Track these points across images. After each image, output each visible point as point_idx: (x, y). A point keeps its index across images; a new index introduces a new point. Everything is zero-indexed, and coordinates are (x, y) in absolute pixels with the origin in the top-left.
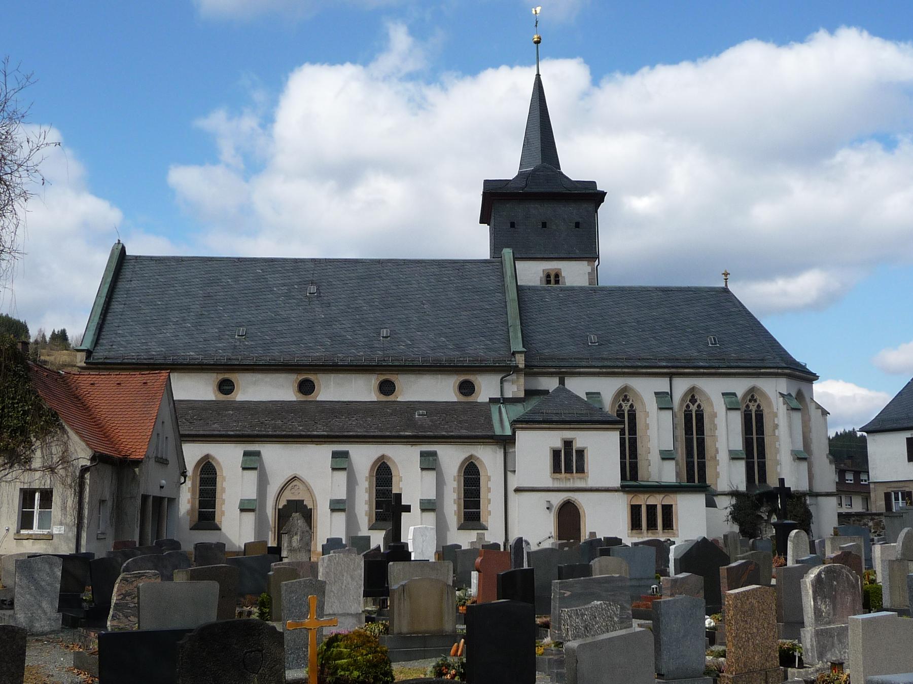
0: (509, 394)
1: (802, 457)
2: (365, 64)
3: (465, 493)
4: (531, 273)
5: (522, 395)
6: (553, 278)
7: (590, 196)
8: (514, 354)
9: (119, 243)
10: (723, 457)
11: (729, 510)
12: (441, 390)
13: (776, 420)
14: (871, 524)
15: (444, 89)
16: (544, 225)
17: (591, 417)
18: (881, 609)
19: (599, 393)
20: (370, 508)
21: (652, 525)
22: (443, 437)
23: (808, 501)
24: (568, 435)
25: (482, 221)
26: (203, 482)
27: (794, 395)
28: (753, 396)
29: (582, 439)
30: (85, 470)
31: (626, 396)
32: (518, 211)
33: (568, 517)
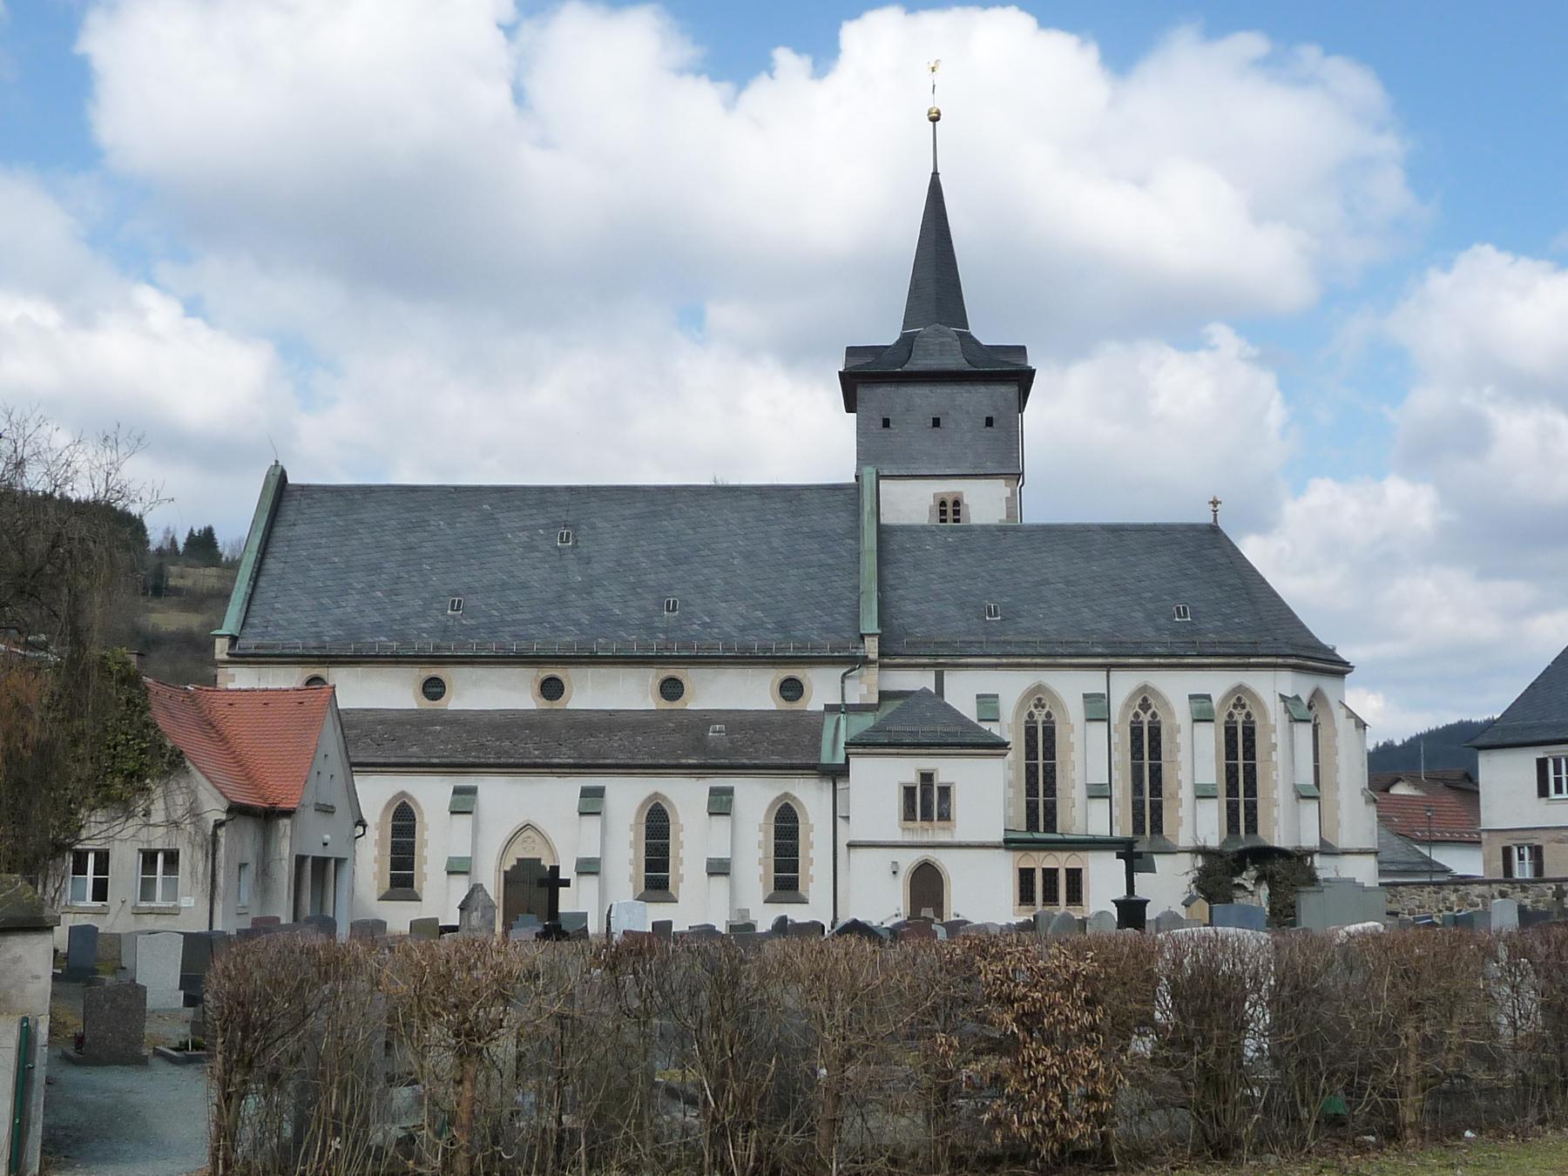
0: (853, 699)
4: (908, 502)
5: (875, 700)
6: (950, 509)
11: (1191, 876)
12: (748, 692)
14: (1453, 898)
16: (936, 423)
17: (974, 742)
18: (508, 926)
20: (766, 872)
21: (1051, 897)
23: (1318, 861)
24: (927, 764)
26: (396, 831)
30: (219, 825)
33: (927, 885)
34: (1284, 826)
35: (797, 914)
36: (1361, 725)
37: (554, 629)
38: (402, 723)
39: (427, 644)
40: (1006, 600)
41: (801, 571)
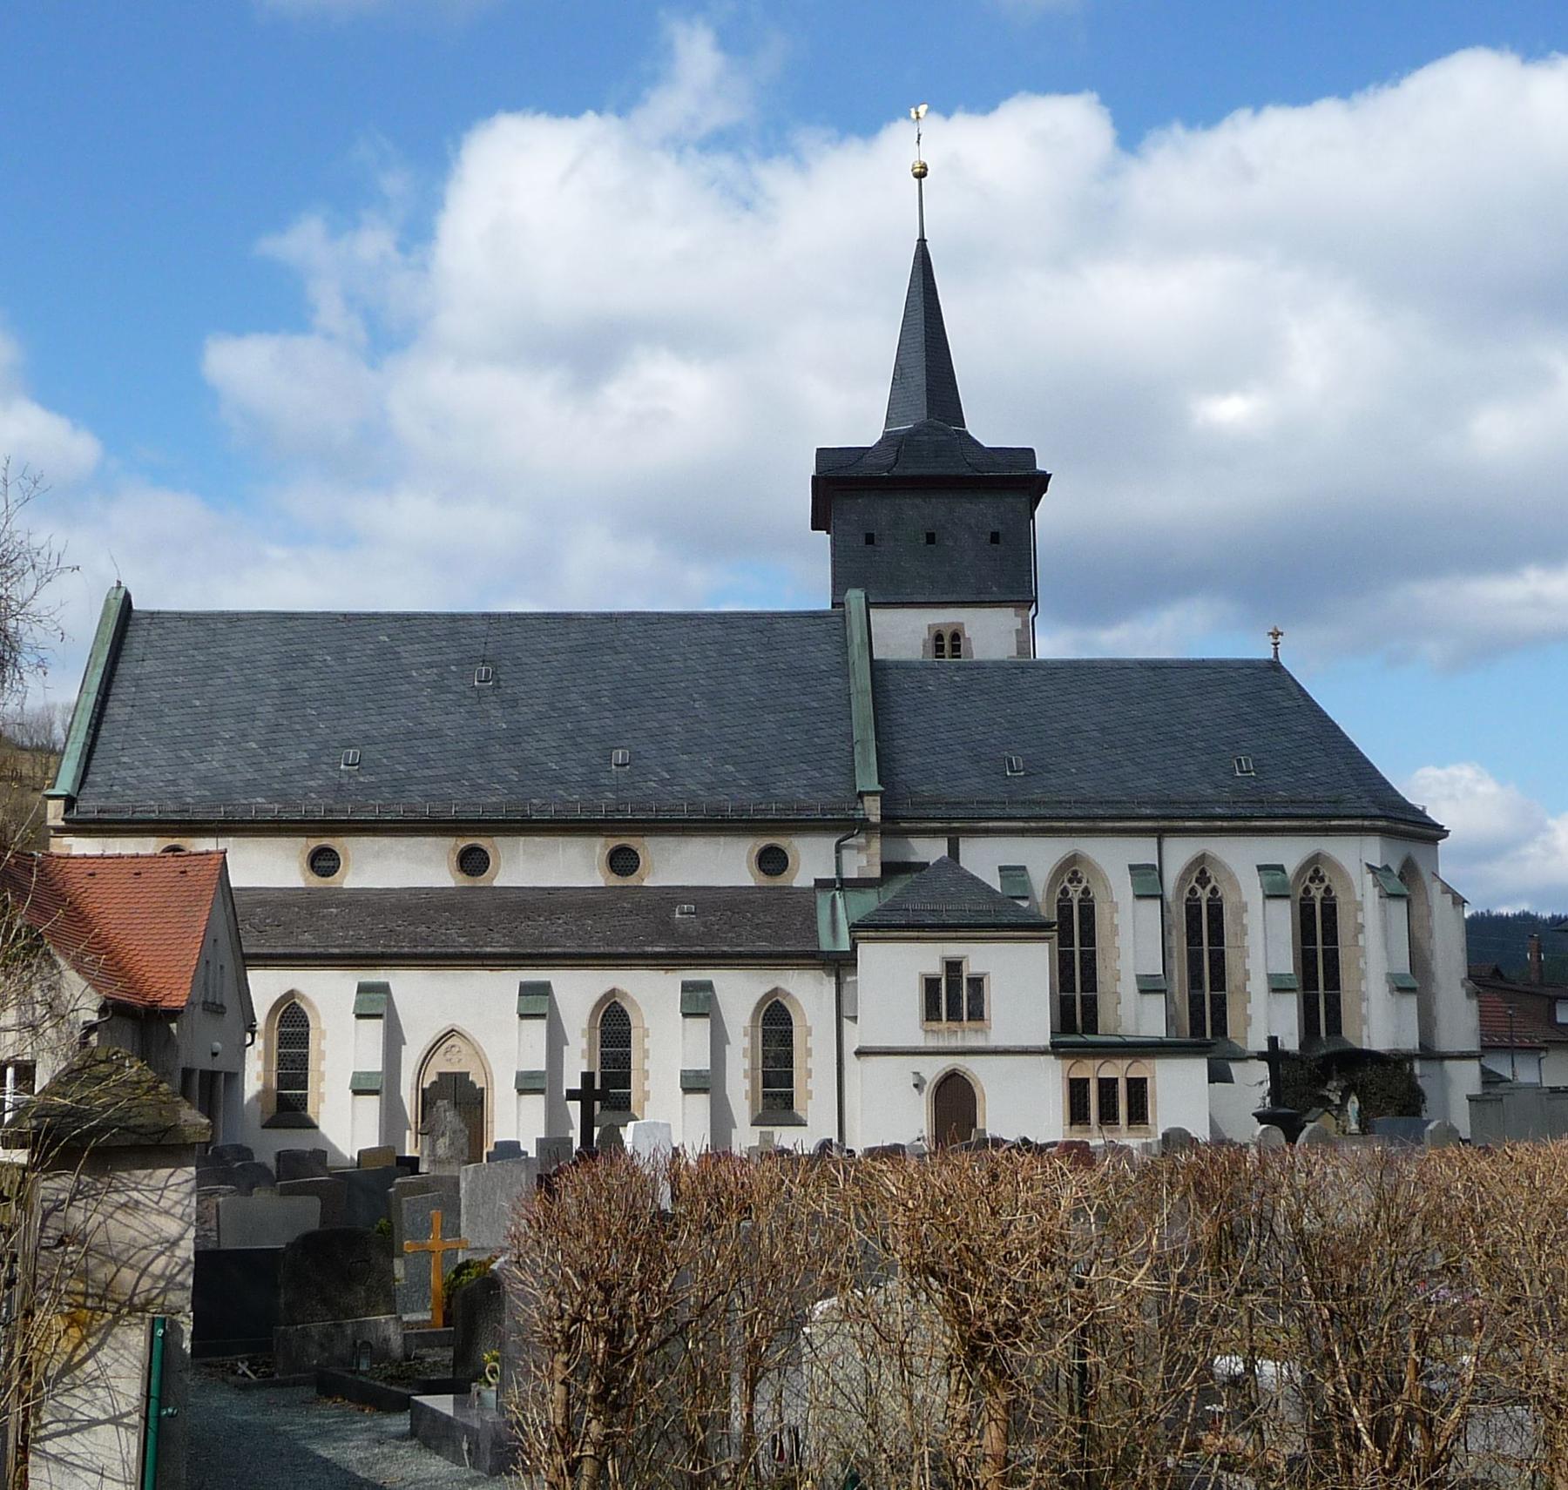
0: (851, 873)
1: (1414, 982)
2: (621, 111)
3: (765, 1058)
4: (902, 633)
5: (876, 872)
6: (948, 643)
7: (1021, 480)
8: (861, 795)
9: (119, 587)
10: (1258, 986)
12: (723, 864)
13: (1360, 915)
15: (801, 165)
17: (1002, 919)
19: (1024, 868)
22: (725, 955)
24: (954, 950)
25: (816, 526)
26: (284, 1040)
27: (1396, 871)
28: (1317, 871)
29: (979, 957)
30: (90, 1028)
31: (1075, 873)
32: (880, 511)
33: (954, 1102)
34: (1379, 1023)
35: (785, 1137)
36: (1459, 902)
37: (475, 787)
38: (285, 905)
39: (317, 806)
40: (1029, 751)
41: (779, 717)
